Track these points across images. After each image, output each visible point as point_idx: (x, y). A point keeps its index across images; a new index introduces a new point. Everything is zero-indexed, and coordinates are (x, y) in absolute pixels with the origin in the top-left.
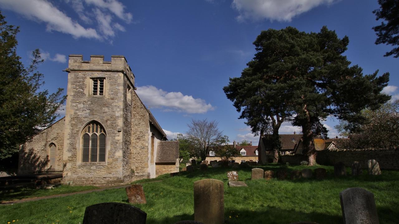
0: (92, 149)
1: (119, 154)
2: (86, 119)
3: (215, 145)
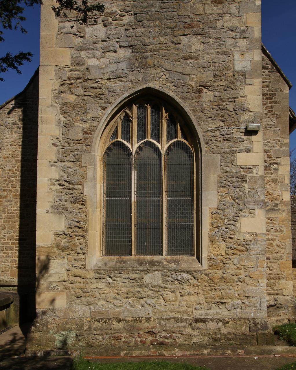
0: (138, 202)
2: (118, 85)
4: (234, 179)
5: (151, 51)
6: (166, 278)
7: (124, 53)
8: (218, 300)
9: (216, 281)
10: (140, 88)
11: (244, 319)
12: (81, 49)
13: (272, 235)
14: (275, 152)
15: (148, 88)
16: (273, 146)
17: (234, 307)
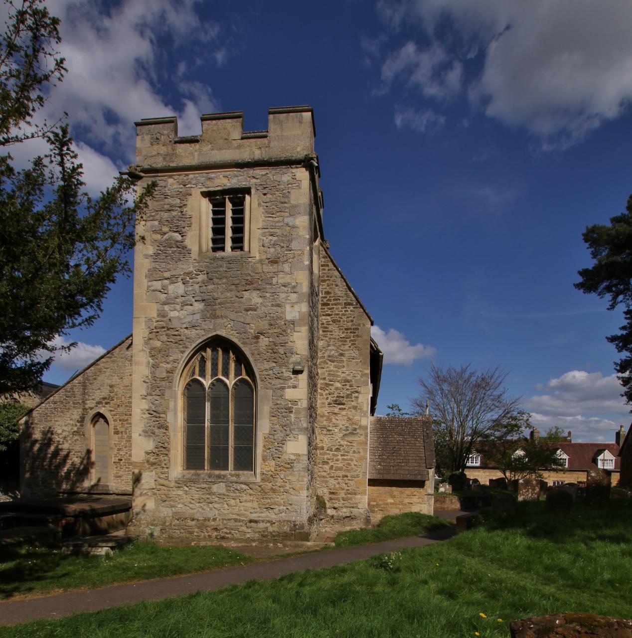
0: (212, 429)
1: (297, 446)
2: (193, 333)
3: (487, 436)
4: (282, 411)
5: (219, 304)
6: (229, 488)
7: (199, 306)
8: (268, 506)
9: (267, 491)
10: (210, 335)
11: (287, 521)
12: (165, 304)
13: (351, 456)
14: (356, 381)
15: (217, 335)
16: (355, 376)
17: (280, 512)
